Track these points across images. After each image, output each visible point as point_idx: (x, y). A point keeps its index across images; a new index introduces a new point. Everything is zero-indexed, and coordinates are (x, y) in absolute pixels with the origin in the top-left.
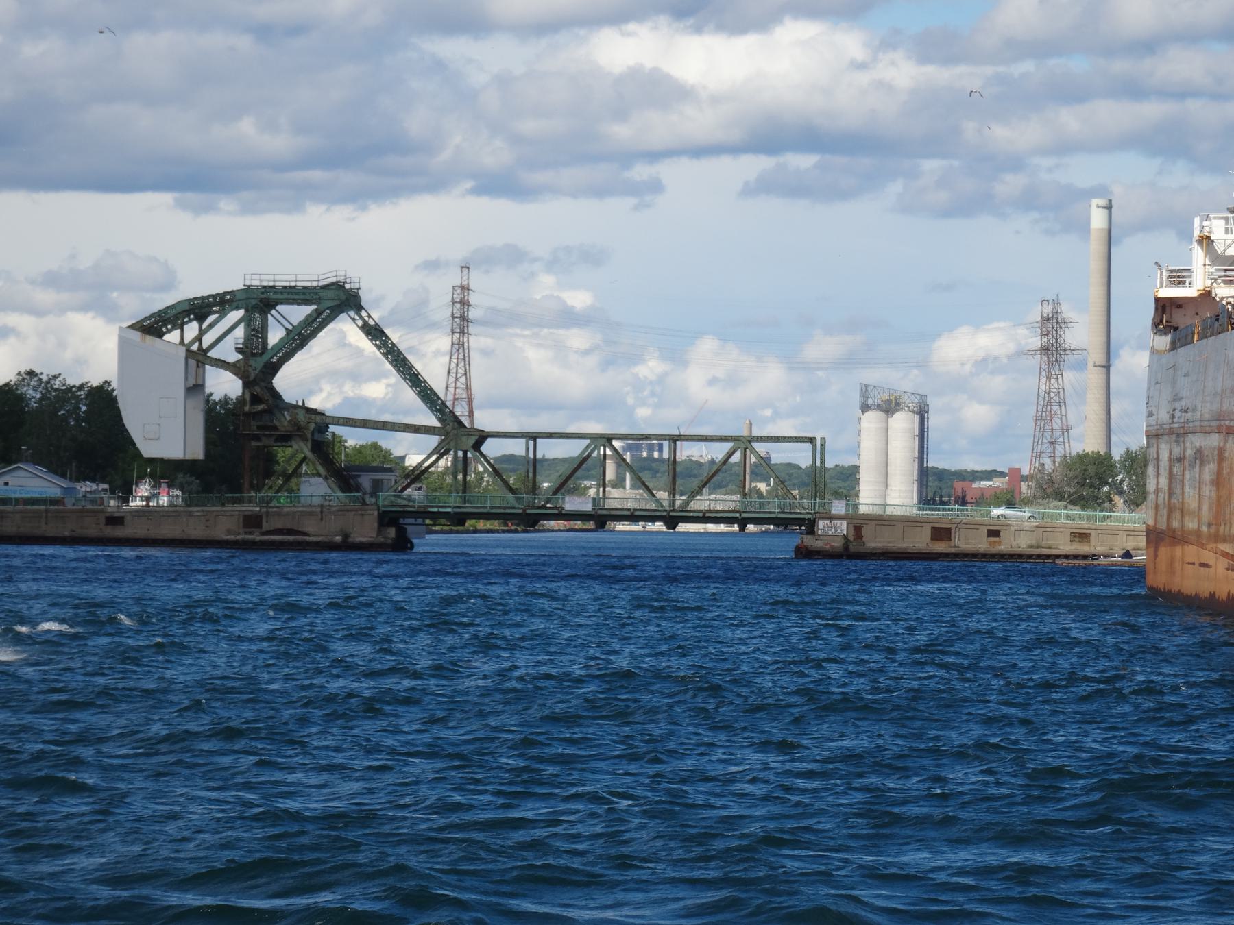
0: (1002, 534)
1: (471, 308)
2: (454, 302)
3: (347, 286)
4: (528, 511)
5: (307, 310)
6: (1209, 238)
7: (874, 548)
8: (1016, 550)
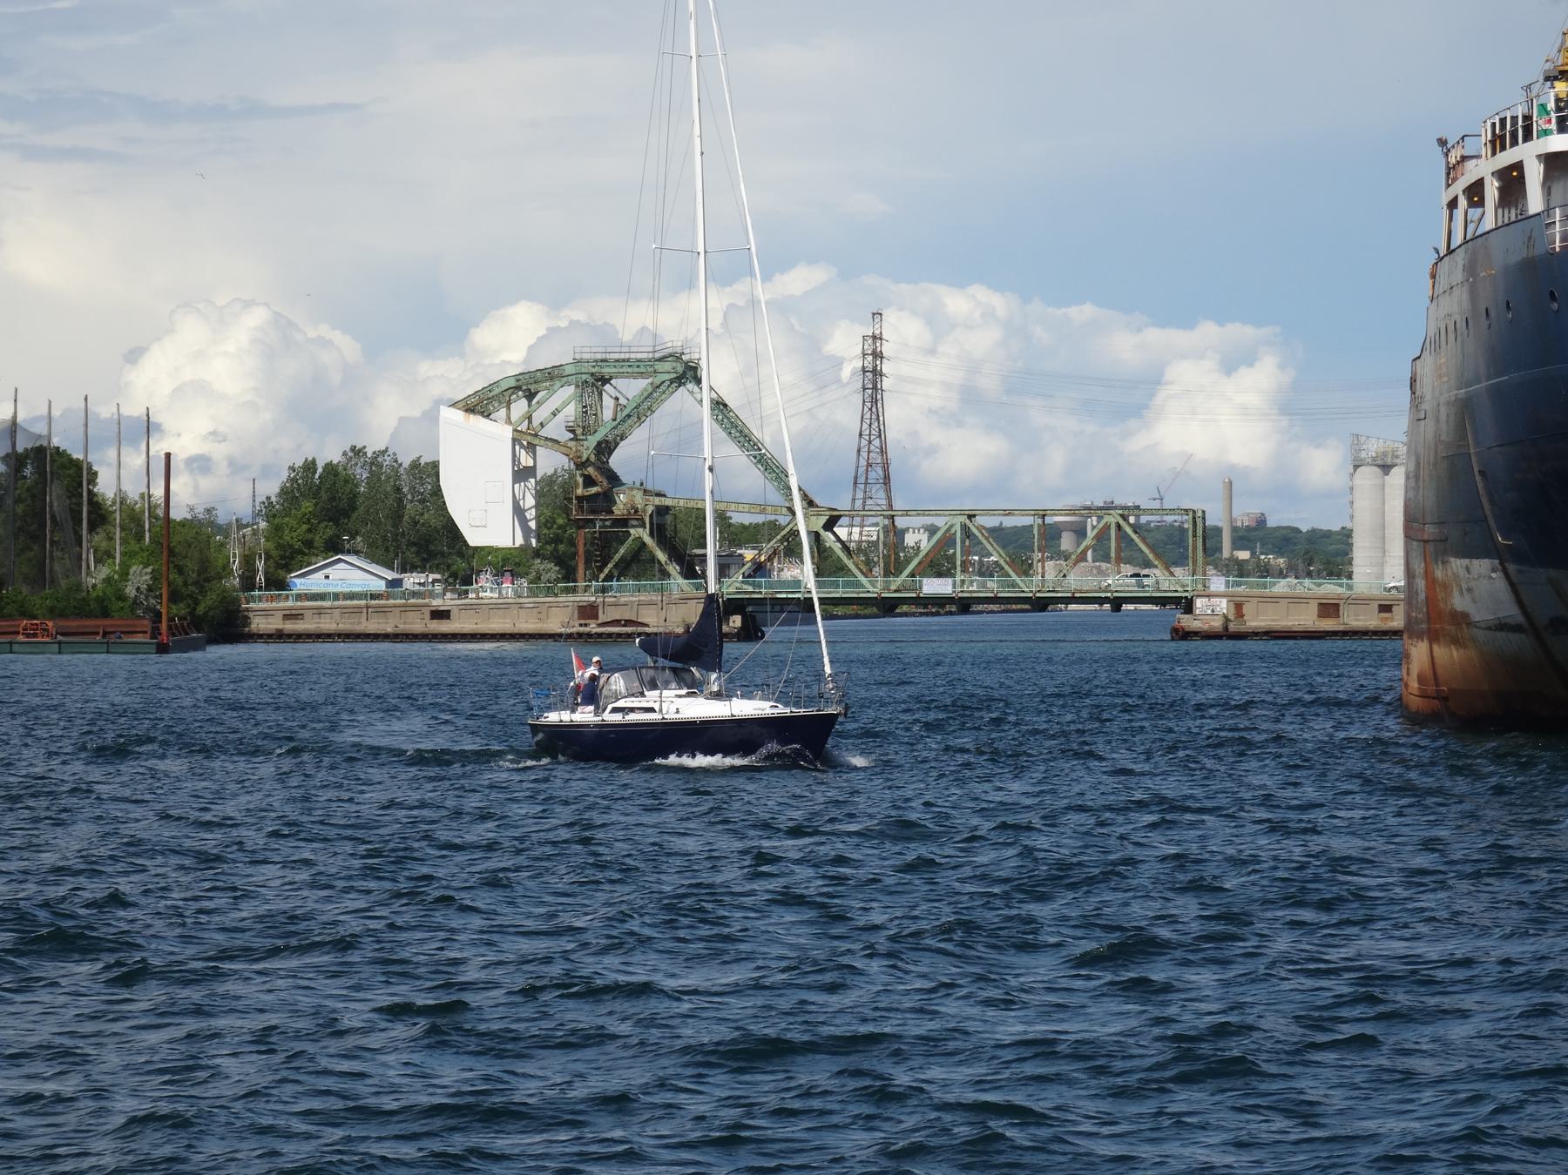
0: (1394, 609)
1: (884, 361)
2: (864, 355)
5: (642, 384)
7: (1256, 627)
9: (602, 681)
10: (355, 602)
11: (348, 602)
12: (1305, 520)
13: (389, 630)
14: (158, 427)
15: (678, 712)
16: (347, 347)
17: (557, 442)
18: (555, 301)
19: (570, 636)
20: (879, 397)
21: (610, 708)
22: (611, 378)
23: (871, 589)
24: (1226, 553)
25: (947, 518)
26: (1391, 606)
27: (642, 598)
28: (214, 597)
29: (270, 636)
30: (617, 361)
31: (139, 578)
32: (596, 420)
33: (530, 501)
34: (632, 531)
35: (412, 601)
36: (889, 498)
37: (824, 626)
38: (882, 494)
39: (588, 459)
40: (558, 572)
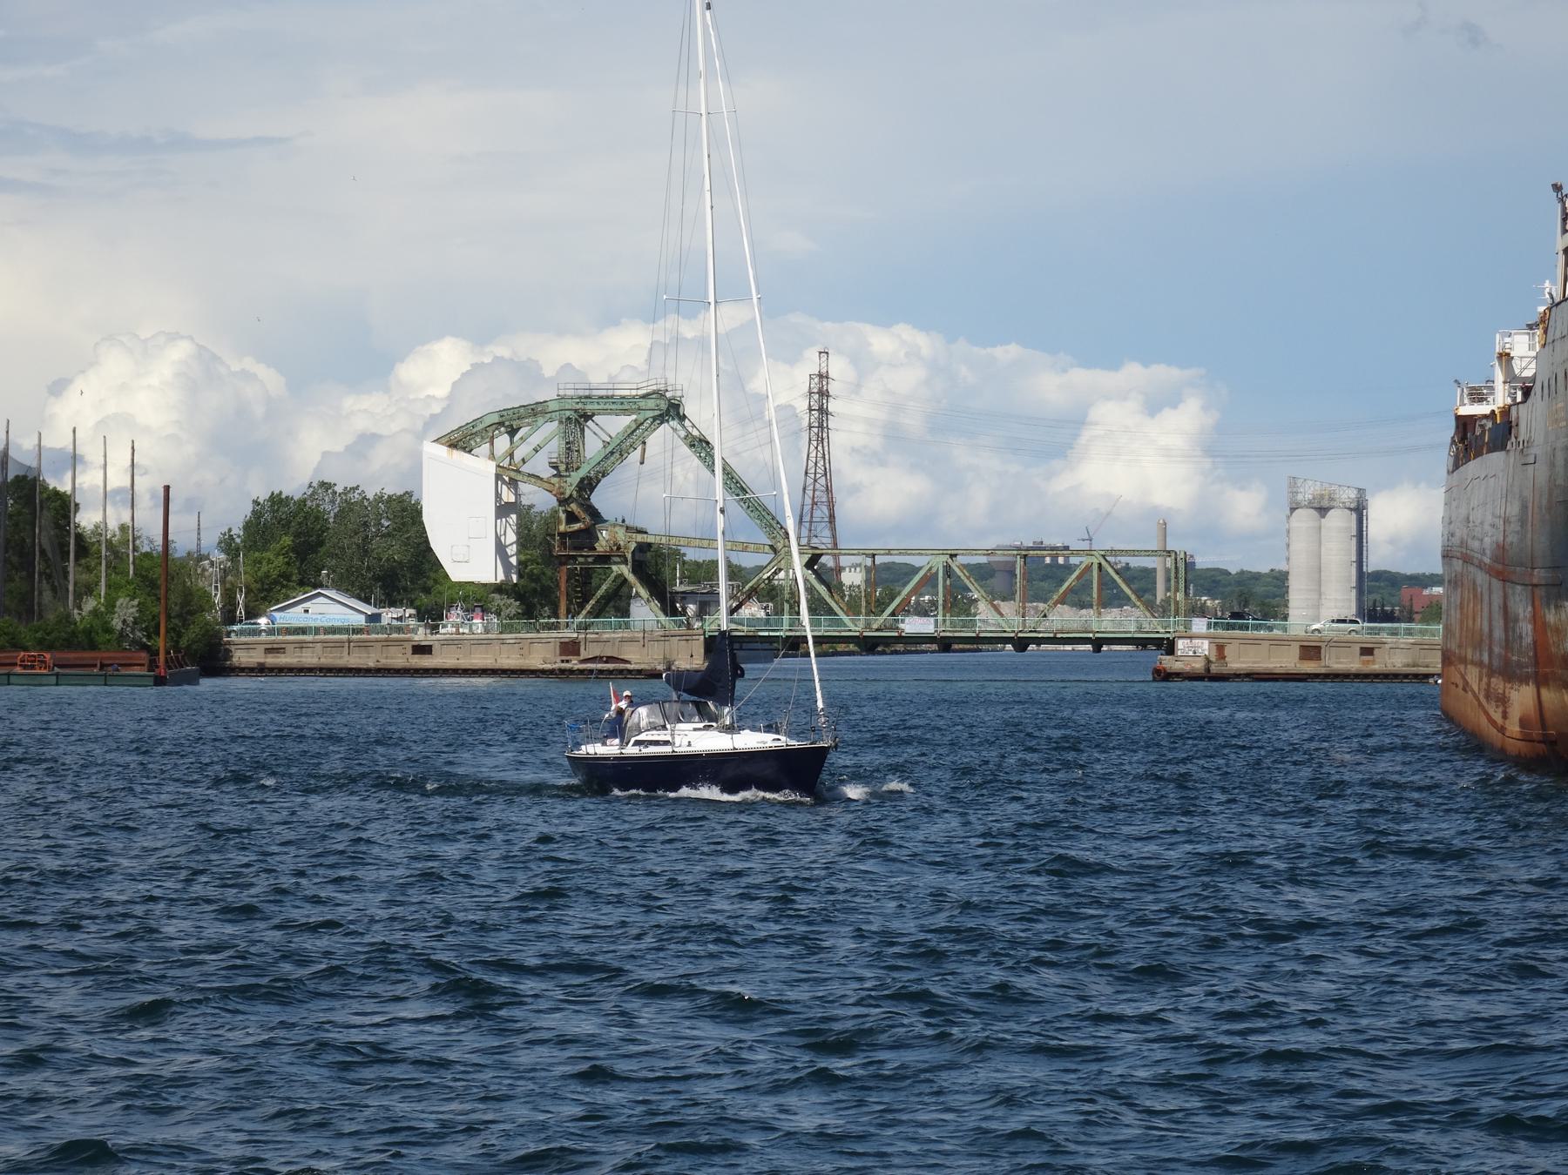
0: (1376, 652)
1: (830, 399)
3: (668, 395)
4: (865, 634)
6: (1508, 354)
8: (1390, 669)
9: (627, 714)
10: (337, 637)
11: (330, 637)
12: (1233, 561)
13: (371, 664)
14: (82, 457)
15: (689, 745)
16: (271, 380)
17: (538, 477)
18: (479, 337)
19: (552, 672)
20: (825, 435)
21: (633, 740)
22: (593, 415)
23: (853, 628)
24: (1160, 594)
25: (929, 558)
26: (1373, 649)
27: (625, 635)
28: (197, 630)
29: (251, 670)
30: (601, 397)
31: (126, 610)
32: (579, 456)
33: (511, 537)
34: (614, 568)
35: (395, 636)
36: (834, 537)
37: (817, 663)
38: (827, 533)
39: (571, 495)
40: (518, 607)
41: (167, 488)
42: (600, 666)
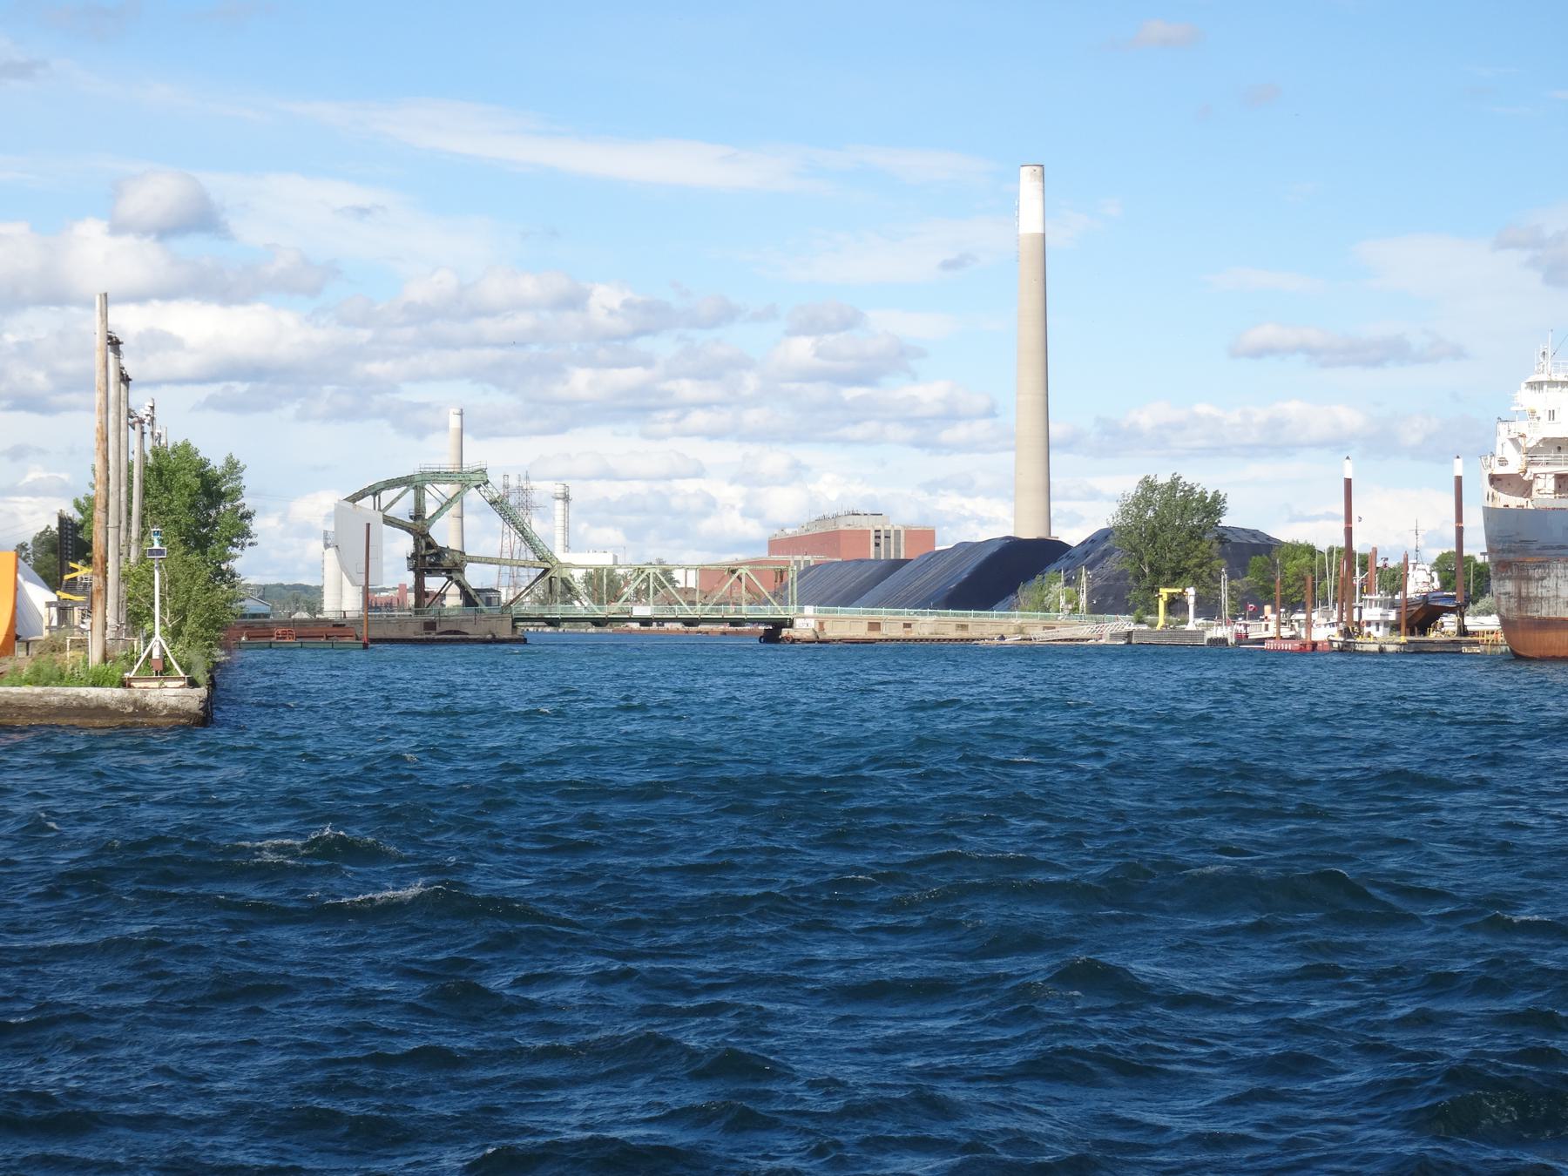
8: (921, 636)
41: (368, 525)
42: (1167, 1045)
